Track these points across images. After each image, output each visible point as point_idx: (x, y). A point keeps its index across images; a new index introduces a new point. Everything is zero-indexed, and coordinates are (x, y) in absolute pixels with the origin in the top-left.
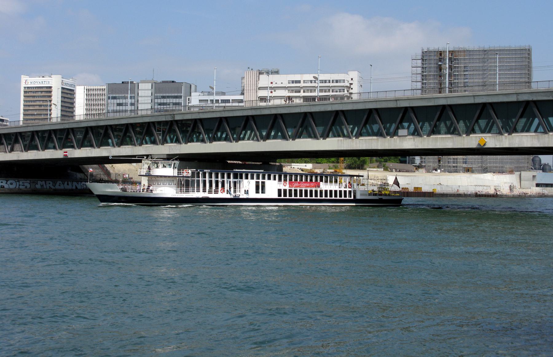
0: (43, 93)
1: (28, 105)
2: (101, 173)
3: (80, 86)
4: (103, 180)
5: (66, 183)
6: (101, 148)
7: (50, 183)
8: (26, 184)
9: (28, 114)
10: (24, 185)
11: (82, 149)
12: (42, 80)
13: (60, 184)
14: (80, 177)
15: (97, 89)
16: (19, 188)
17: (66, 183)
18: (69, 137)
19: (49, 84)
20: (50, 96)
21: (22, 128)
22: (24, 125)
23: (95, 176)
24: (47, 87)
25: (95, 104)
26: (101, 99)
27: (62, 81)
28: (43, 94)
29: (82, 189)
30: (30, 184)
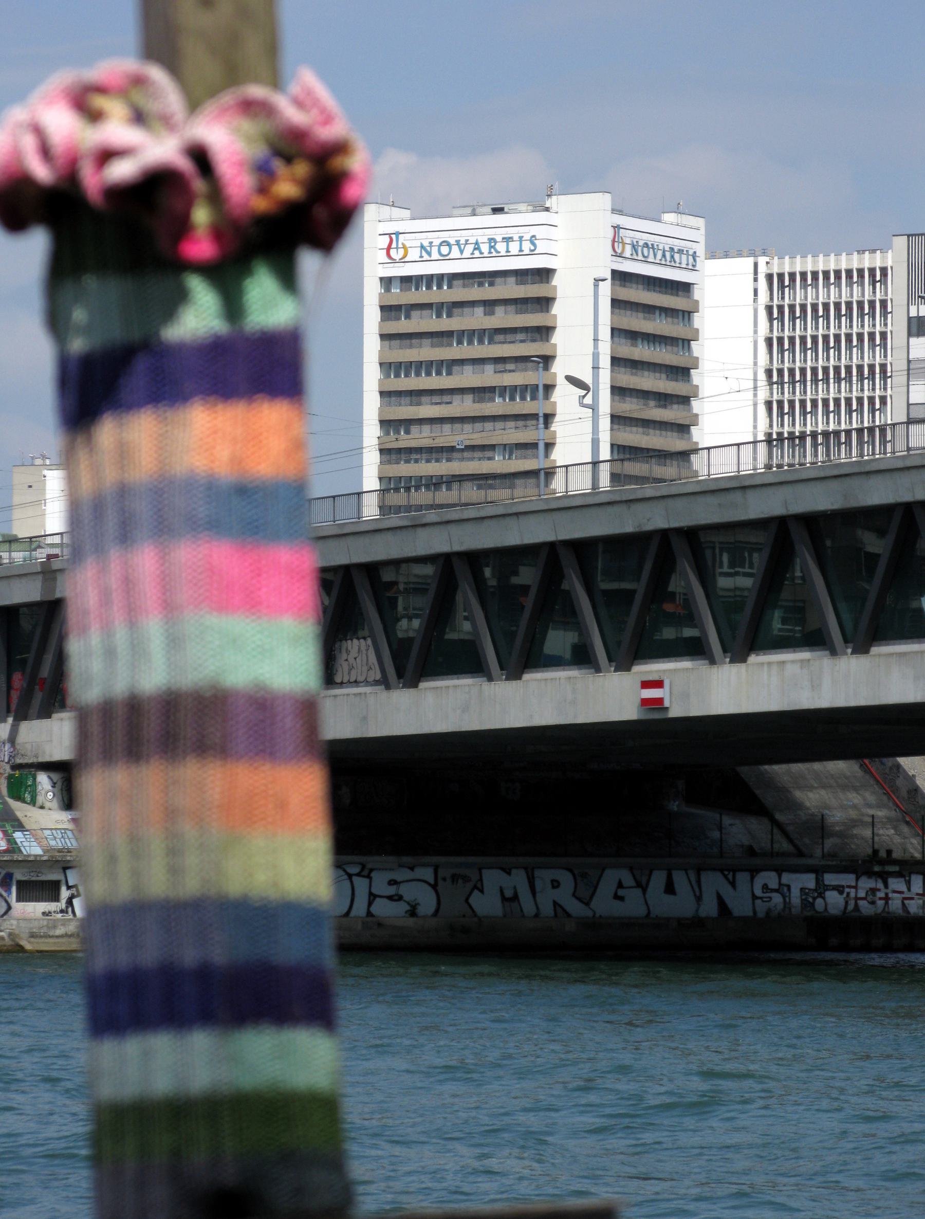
0: (500, 310)
1: (411, 393)
2: (880, 813)
3: (726, 256)
4: (889, 859)
5: (658, 879)
6: (875, 650)
7: (555, 884)
8: (409, 891)
9: (410, 450)
10: (400, 898)
11: (753, 659)
12: (490, 233)
13: (620, 885)
14: (746, 841)
15: (861, 272)
16: (369, 914)
17: (658, 879)
18: (675, 585)
19: (532, 253)
20: (545, 332)
21: (378, 537)
22: (395, 520)
23: (841, 835)
24: (522, 275)
25: (826, 370)
26: (860, 336)
27: (616, 228)
28: (502, 318)
29: (761, 914)
30: (434, 887)
